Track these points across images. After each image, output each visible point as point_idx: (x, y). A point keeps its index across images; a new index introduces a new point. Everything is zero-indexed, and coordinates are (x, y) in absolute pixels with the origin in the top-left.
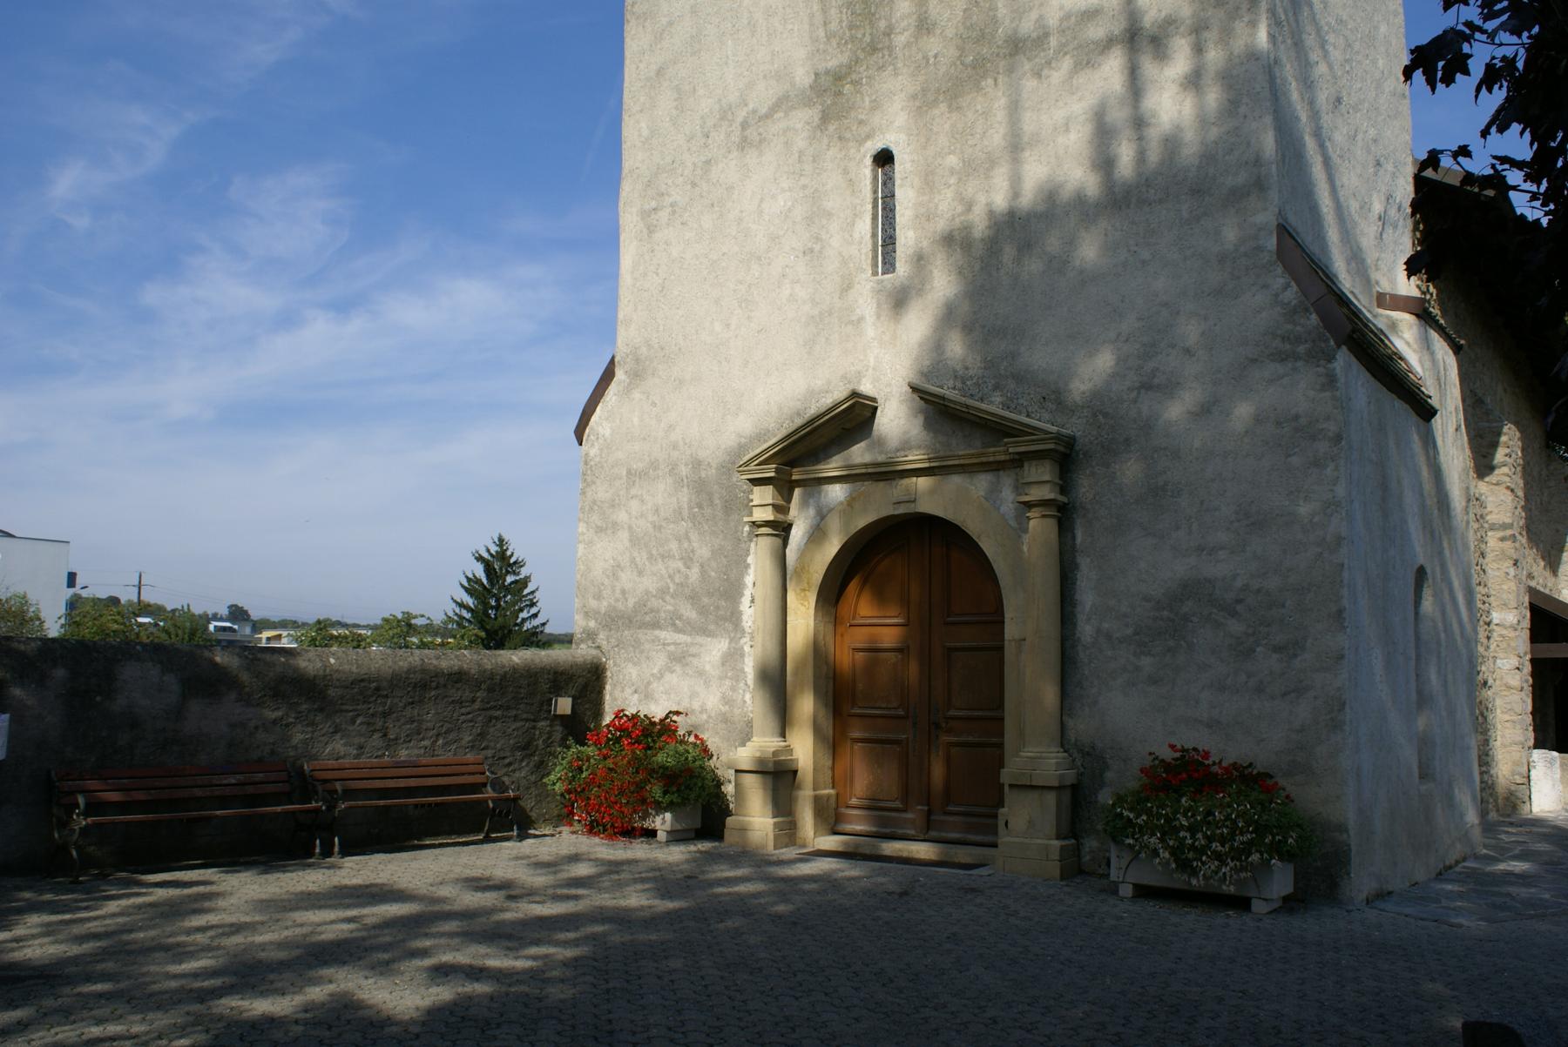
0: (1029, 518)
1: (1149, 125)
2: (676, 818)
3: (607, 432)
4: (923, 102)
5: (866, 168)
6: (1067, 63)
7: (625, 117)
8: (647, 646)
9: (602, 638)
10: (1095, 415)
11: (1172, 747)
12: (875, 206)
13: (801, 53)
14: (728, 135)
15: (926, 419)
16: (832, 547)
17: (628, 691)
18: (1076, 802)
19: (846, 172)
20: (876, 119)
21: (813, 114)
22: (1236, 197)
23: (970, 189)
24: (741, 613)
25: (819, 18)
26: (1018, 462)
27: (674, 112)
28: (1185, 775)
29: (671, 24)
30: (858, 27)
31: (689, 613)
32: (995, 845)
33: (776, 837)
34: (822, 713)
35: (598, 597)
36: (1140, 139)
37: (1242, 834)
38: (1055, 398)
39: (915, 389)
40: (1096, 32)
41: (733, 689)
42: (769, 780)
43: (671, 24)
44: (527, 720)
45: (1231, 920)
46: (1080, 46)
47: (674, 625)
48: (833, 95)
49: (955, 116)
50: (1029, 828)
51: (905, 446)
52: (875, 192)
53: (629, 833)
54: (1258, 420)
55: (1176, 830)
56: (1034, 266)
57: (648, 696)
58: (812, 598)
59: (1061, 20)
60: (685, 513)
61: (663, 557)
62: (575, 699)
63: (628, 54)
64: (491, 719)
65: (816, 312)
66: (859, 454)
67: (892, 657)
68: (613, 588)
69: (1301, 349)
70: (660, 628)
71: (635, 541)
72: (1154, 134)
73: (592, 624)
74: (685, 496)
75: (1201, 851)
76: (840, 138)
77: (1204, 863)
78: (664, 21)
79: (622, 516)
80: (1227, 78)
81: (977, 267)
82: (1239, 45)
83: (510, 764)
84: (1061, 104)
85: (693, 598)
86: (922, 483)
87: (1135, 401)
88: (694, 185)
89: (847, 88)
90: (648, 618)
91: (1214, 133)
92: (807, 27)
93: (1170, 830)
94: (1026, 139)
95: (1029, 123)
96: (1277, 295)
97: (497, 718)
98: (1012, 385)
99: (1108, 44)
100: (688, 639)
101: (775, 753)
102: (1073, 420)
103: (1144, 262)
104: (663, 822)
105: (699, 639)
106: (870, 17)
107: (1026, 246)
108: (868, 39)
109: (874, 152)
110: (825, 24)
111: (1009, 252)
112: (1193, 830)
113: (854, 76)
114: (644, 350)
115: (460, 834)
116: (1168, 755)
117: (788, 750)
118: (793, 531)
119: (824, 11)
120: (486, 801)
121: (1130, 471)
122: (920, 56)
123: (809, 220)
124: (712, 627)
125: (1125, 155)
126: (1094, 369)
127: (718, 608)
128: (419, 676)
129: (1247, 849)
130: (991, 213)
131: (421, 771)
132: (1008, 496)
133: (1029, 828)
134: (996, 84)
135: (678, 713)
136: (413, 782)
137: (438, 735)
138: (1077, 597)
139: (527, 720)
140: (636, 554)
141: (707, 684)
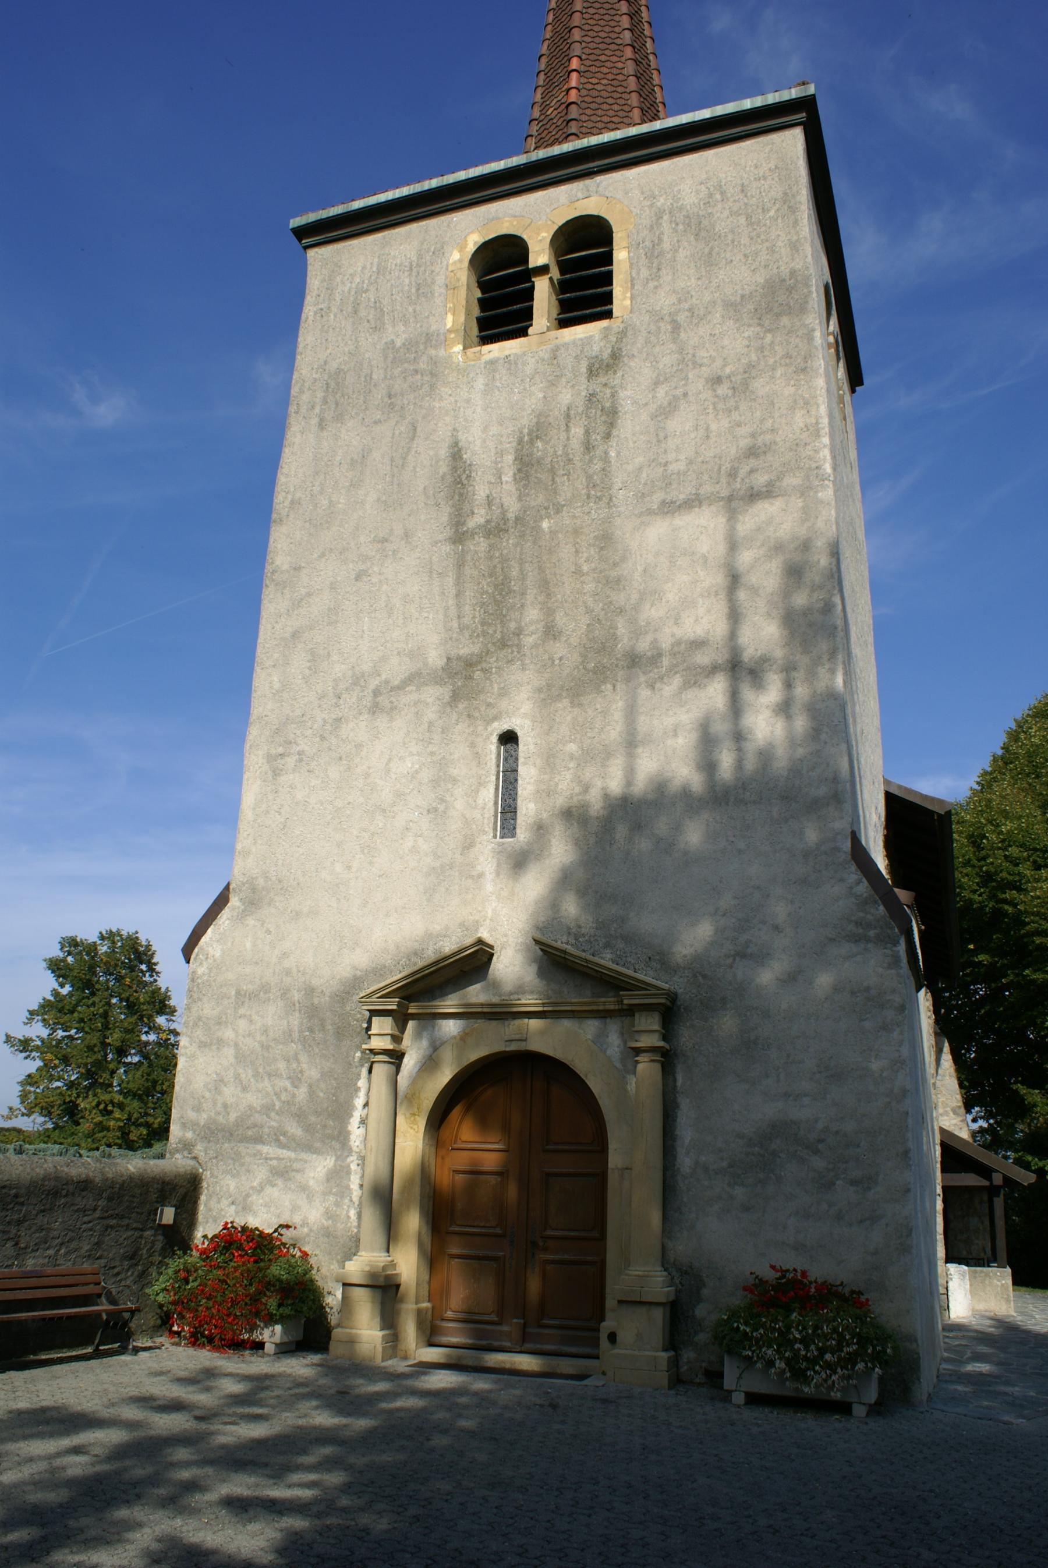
0: (637, 1062)
1: (746, 739)
2: (285, 1331)
3: (218, 954)
4: (547, 696)
5: (492, 746)
6: (677, 681)
7: (258, 669)
8: (248, 1159)
9: (199, 1149)
10: (695, 976)
11: (773, 1267)
12: (498, 779)
13: (435, 639)
14: (360, 699)
15: (540, 968)
16: (445, 1076)
17: (225, 1202)
18: (678, 1315)
19: (473, 745)
20: (504, 704)
21: (444, 692)
22: (814, 806)
23: (589, 772)
24: (349, 1133)
25: (453, 611)
26: (630, 1011)
27: (307, 672)
28: (784, 1296)
29: (309, 595)
30: (490, 624)
31: (295, 1130)
32: (597, 1357)
33: (384, 1349)
34: (424, 1230)
35: (198, 1109)
36: (739, 749)
37: (848, 1345)
38: (661, 959)
39: (537, 942)
40: (703, 659)
41: (337, 1204)
42: (378, 1294)
43: (309, 595)
44: (136, 1229)
45: (836, 1422)
46: (688, 668)
47: (278, 1140)
48: (464, 679)
49: (576, 711)
50: (635, 1343)
51: (520, 990)
52: (498, 766)
53: (238, 1345)
54: (836, 989)
55: (791, 1343)
56: (644, 844)
57: (246, 1208)
58: (422, 1123)
59: (673, 645)
60: (296, 1035)
61: (269, 1075)
62: (177, 1207)
63: (264, 614)
64: (108, 1227)
65: (437, 864)
66: (476, 994)
67: (493, 1180)
68: (215, 1104)
69: (872, 933)
70: (263, 1143)
71: (241, 1058)
72: (750, 747)
73: (189, 1135)
74: (296, 1020)
75: (813, 1361)
76: (469, 716)
77: (816, 1372)
78: (303, 591)
79: (228, 1034)
80: (812, 710)
81: (592, 840)
82: (821, 685)
83: (118, 1274)
84: (671, 713)
85: (300, 1116)
86: (534, 1024)
87: (731, 967)
88: (323, 738)
89: (478, 675)
90: (250, 1133)
91: (800, 752)
92: (441, 617)
93: (784, 1341)
94: (639, 738)
95: (643, 724)
96: (851, 888)
97: (112, 1227)
98: (620, 944)
99: (714, 669)
100: (292, 1155)
101: (384, 1268)
102: (676, 978)
103: (740, 851)
104: (272, 1335)
105: (304, 1155)
106: (502, 619)
107: (637, 827)
108: (498, 636)
109: (500, 731)
110: (459, 617)
111: (621, 831)
112: (806, 1342)
113: (484, 665)
114: (261, 881)
115: (71, 1346)
116: (770, 1275)
117: (393, 1265)
118: (406, 1060)
119: (459, 606)
120: (98, 1314)
121: (727, 1024)
122: (546, 657)
123: (435, 783)
124: (318, 1145)
125: (726, 760)
126: (696, 937)
127: (325, 1126)
128: (53, 1183)
129: (851, 1360)
130: (606, 796)
131: (46, 1281)
132: (614, 1041)
133: (635, 1343)
134: (614, 690)
135: (288, 1227)
136: (39, 1294)
137: (62, 1244)
138: (678, 1132)
139: (136, 1229)
140: (241, 1071)
141: (310, 1198)
